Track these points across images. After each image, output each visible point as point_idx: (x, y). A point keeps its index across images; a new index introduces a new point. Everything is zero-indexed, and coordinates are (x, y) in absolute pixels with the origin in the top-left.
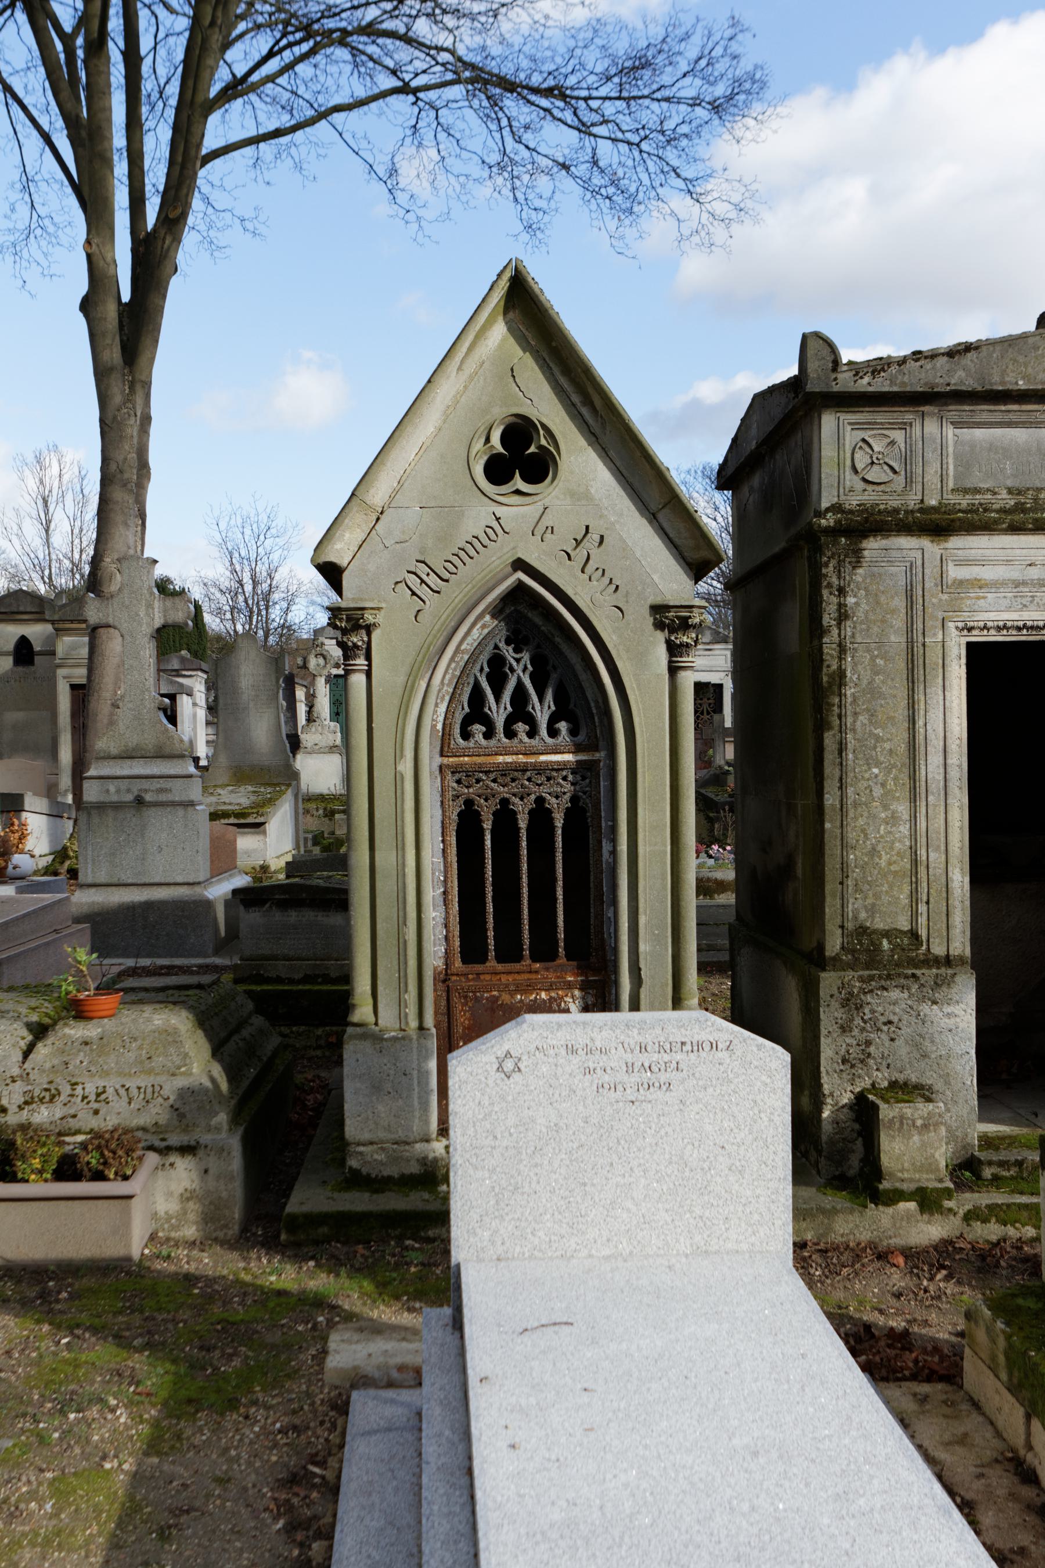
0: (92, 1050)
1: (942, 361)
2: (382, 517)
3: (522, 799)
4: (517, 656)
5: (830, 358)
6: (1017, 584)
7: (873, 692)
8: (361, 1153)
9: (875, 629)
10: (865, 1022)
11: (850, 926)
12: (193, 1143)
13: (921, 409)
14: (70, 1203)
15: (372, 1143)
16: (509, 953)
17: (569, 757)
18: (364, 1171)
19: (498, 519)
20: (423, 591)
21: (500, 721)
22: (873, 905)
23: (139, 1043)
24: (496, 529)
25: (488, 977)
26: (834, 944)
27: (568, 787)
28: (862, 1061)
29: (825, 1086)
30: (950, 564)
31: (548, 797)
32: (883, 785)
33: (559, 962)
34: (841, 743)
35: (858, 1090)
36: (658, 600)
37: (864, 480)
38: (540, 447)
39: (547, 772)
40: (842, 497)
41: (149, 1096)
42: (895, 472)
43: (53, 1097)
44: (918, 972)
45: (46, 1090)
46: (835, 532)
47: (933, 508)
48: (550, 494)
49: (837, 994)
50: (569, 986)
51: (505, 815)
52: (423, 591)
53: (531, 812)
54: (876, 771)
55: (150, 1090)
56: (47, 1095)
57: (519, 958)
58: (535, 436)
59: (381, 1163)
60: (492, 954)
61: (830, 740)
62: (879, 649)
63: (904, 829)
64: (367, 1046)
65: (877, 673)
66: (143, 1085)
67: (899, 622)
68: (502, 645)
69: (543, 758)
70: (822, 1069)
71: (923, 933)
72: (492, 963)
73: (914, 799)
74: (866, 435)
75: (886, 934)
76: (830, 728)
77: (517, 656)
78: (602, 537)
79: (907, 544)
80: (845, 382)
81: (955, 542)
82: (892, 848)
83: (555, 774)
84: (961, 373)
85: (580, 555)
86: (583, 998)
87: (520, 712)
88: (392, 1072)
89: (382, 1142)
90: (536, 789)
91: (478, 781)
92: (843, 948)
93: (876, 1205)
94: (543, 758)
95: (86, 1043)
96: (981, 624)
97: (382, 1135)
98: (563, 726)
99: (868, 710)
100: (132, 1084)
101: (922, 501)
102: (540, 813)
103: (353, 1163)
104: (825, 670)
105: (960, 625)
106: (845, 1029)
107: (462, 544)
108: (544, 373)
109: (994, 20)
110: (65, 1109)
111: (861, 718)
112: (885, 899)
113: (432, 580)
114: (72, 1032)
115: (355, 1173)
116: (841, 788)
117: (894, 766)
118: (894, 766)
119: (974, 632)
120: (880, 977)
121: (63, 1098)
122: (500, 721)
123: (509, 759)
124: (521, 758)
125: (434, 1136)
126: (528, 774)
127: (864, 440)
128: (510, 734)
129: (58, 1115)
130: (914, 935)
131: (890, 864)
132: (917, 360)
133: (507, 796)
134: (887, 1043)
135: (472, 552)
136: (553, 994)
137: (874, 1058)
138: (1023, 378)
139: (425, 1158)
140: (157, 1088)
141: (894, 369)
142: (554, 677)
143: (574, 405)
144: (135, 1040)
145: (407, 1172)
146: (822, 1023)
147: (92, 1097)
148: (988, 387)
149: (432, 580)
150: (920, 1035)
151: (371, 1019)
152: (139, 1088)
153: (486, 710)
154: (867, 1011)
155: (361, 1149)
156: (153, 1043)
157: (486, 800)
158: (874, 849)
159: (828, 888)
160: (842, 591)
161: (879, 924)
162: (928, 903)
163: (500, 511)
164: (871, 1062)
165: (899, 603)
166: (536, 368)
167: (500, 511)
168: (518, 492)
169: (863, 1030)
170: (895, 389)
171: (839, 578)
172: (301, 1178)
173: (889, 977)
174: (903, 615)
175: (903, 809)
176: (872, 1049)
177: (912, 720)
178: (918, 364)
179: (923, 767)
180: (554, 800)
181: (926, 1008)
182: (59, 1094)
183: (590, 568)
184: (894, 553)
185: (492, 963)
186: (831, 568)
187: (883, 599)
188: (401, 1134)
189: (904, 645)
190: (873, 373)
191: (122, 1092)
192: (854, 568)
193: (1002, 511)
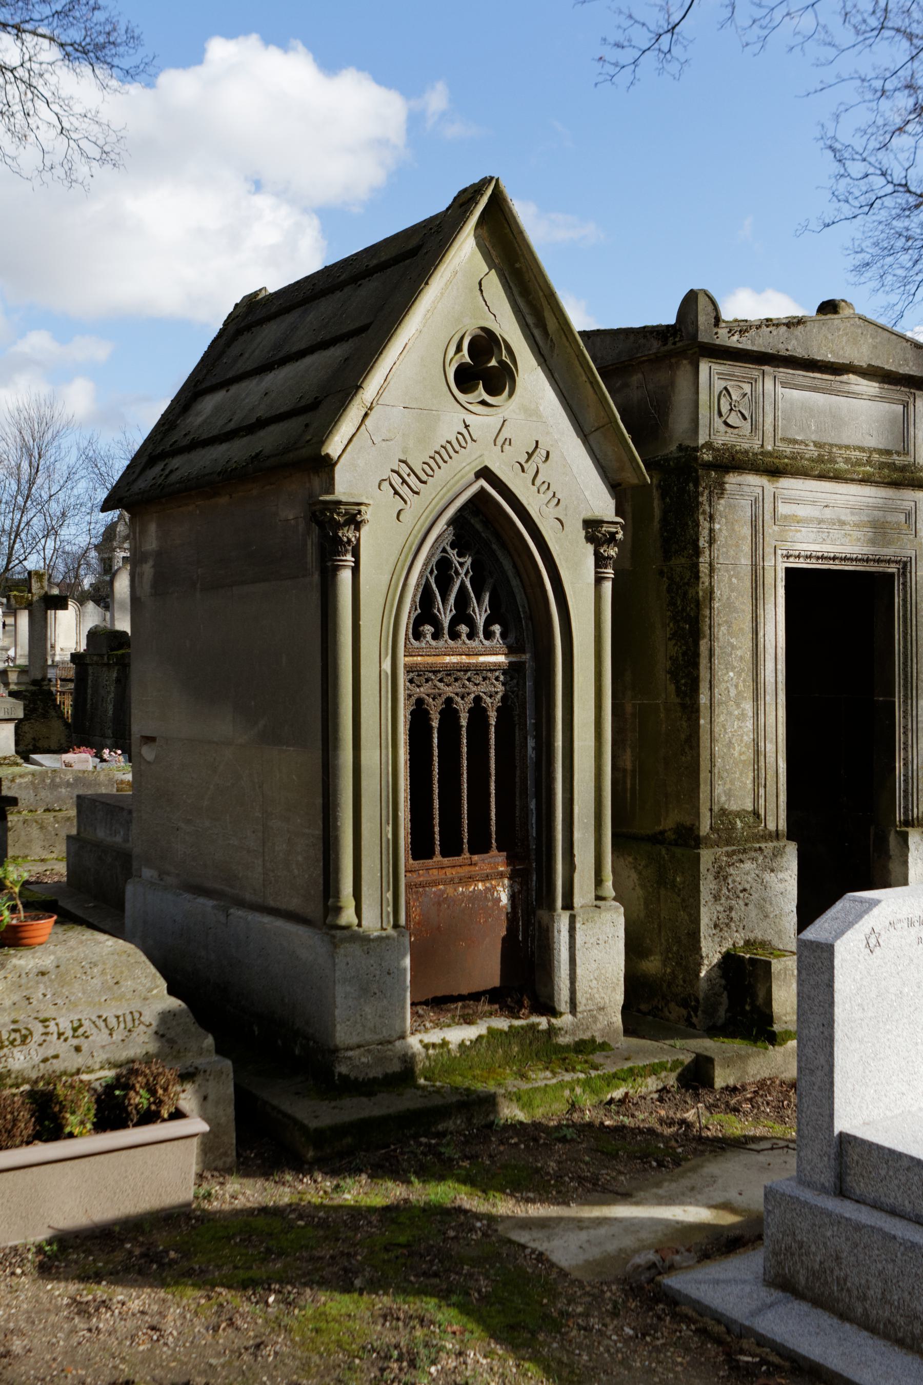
0: (51, 980)
1: (784, 328)
2: (373, 414)
3: (463, 698)
4: (461, 560)
5: (713, 315)
6: (820, 521)
7: (729, 605)
8: (350, 1058)
9: (732, 553)
10: (729, 891)
11: (716, 808)
12: (191, 1070)
13: (763, 368)
14: (132, 1151)
15: (359, 1047)
16: (451, 849)
17: (501, 659)
18: (352, 1076)
19: (467, 426)
20: (404, 490)
21: (480, 620)
22: (730, 789)
23: (100, 967)
24: (466, 435)
25: (435, 872)
26: (705, 828)
27: (500, 688)
28: (727, 925)
29: (703, 949)
30: (780, 501)
31: (485, 697)
32: (736, 686)
33: (491, 853)
34: (711, 650)
35: (724, 950)
36: (589, 515)
37: (726, 423)
38: (501, 362)
39: (482, 671)
40: (712, 437)
41: (129, 1025)
42: (745, 419)
43: (24, 1039)
44: (763, 845)
45: (15, 1031)
46: (709, 466)
47: (769, 452)
48: (508, 407)
49: (712, 869)
50: (501, 875)
51: (449, 713)
52: (404, 490)
53: (470, 711)
54: (731, 674)
55: (129, 1018)
56: (17, 1035)
57: (459, 852)
58: (496, 351)
59: (367, 1065)
60: (438, 849)
61: (704, 645)
62: (734, 569)
63: (749, 724)
64: (355, 949)
65: (732, 591)
66: (120, 1013)
67: (746, 548)
68: (448, 548)
69: (482, 659)
70: (702, 934)
71: (762, 812)
72: (438, 858)
73: (756, 699)
74: (729, 385)
75: (738, 814)
76: (704, 637)
77: (461, 560)
78: (548, 453)
79: (753, 480)
80: (724, 338)
81: (786, 483)
82: (741, 741)
83: (489, 675)
84: (794, 342)
85: (531, 468)
86: (511, 886)
87: (462, 616)
88: (378, 972)
89: (369, 1044)
90: (475, 688)
91: (427, 681)
92: (711, 828)
93: (773, 1045)
94: (482, 659)
95: (43, 974)
96: (797, 553)
97: (368, 1037)
98: (497, 628)
99: (726, 622)
100: (109, 1013)
101: (762, 446)
102: (478, 711)
103: (343, 1069)
104: (701, 585)
105: (785, 552)
106: (717, 898)
107: (438, 448)
108: (506, 293)
109: (360, 68)
110: (41, 1050)
111: (722, 628)
112: (737, 784)
113: (412, 480)
114: (22, 962)
115: (344, 1078)
116: (711, 688)
117: (743, 670)
118: (743, 670)
119: (791, 559)
120: (739, 852)
121: (37, 1037)
122: (480, 620)
123: (455, 659)
124: (465, 659)
125: (409, 1032)
126: (469, 674)
127: (726, 388)
128: (454, 635)
129: (37, 1059)
130: (756, 814)
131: (740, 754)
132: (767, 326)
133: (452, 695)
134: (743, 908)
135: (446, 457)
136: (488, 885)
137: (735, 922)
138: (831, 353)
139: (405, 1055)
140: (136, 1015)
141: (753, 332)
142: (490, 581)
143: (527, 325)
144: (96, 965)
145: (389, 1071)
146: (702, 894)
147: (69, 1033)
148: (811, 356)
149: (412, 480)
150: (763, 899)
151: (355, 921)
152: (118, 1017)
153: (436, 611)
154: (730, 881)
155: (350, 1053)
156: (115, 966)
157: (434, 699)
158: (730, 742)
159: (702, 776)
160: (712, 518)
161: (734, 806)
162: (765, 787)
163: (470, 419)
164: (733, 925)
165: (747, 531)
166: (500, 286)
167: (470, 419)
168: (483, 403)
169: (728, 898)
170: (755, 348)
171: (710, 506)
172: (796, 1049)
173: (745, 851)
174: (749, 541)
175: (748, 706)
176: (733, 914)
177: (756, 632)
178: (769, 329)
179: (762, 671)
180: (488, 700)
181: (769, 877)
182: (31, 1034)
183: (538, 481)
184: (746, 489)
185: (438, 858)
186: (705, 498)
187: (736, 528)
188: (385, 1033)
189: (750, 567)
190: (740, 331)
191: (101, 1024)
192: (719, 498)
193: (811, 460)
